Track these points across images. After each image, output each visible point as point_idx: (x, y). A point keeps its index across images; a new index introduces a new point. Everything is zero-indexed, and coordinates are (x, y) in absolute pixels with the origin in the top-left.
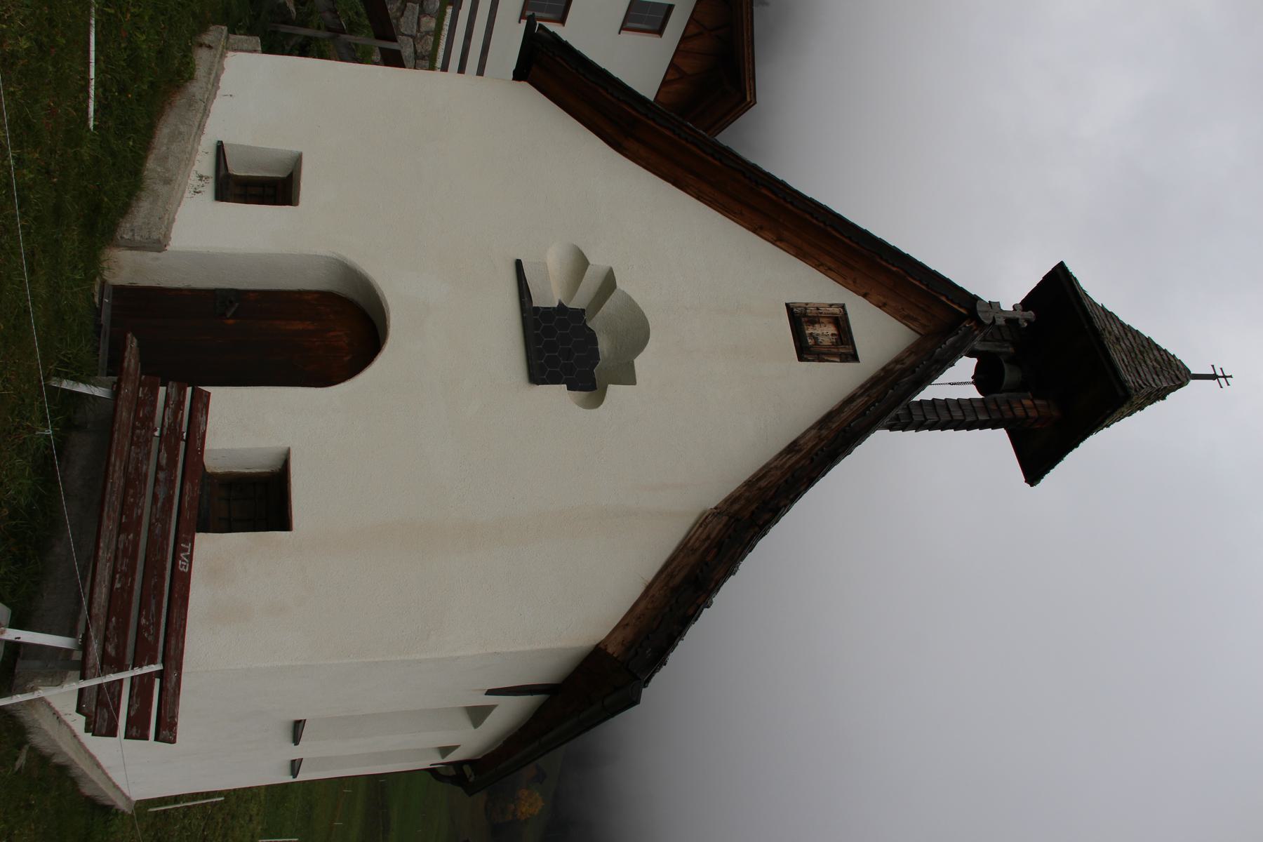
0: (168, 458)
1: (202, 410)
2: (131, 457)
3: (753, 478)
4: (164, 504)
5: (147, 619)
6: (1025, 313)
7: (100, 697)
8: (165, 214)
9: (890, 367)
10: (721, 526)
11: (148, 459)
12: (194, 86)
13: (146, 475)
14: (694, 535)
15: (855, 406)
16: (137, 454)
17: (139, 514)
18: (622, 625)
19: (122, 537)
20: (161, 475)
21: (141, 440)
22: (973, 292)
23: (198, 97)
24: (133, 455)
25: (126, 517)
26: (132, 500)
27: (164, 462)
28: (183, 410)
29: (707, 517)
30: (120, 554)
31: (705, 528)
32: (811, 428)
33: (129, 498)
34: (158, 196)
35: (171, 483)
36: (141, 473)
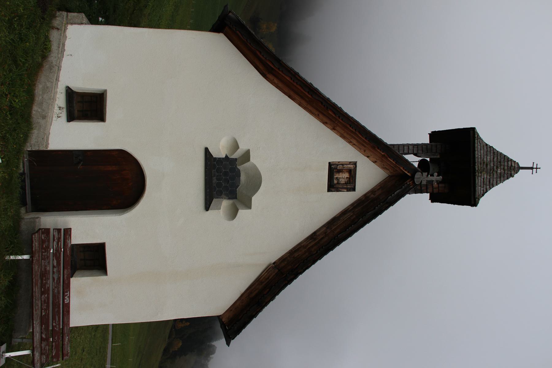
0: (57, 262)
1: (69, 238)
2: (43, 265)
3: (293, 250)
4: (57, 281)
5: (55, 323)
6: (438, 177)
7: (42, 352)
8: (44, 136)
9: (368, 195)
10: (274, 274)
11: (49, 264)
12: (52, 56)
13: (49, 271)
14: (264, 275)
15: (346, 217)
16: (45, 263)
17: (48, 286)
18: (229, 310)
19: (43, 296)
20: (55, 270)
21: (45, 257)
23: (54, 63)
24: (43, 264)
25: (43, 289)
26: (45, 282)
27: (55, 264)
28: (61, 241)
29: (270, 269)
30: (43, 303)
31: (268, 273)
33: (44, 281)
34: (41, 126)
35: (59, 272)
36: (47, 271)
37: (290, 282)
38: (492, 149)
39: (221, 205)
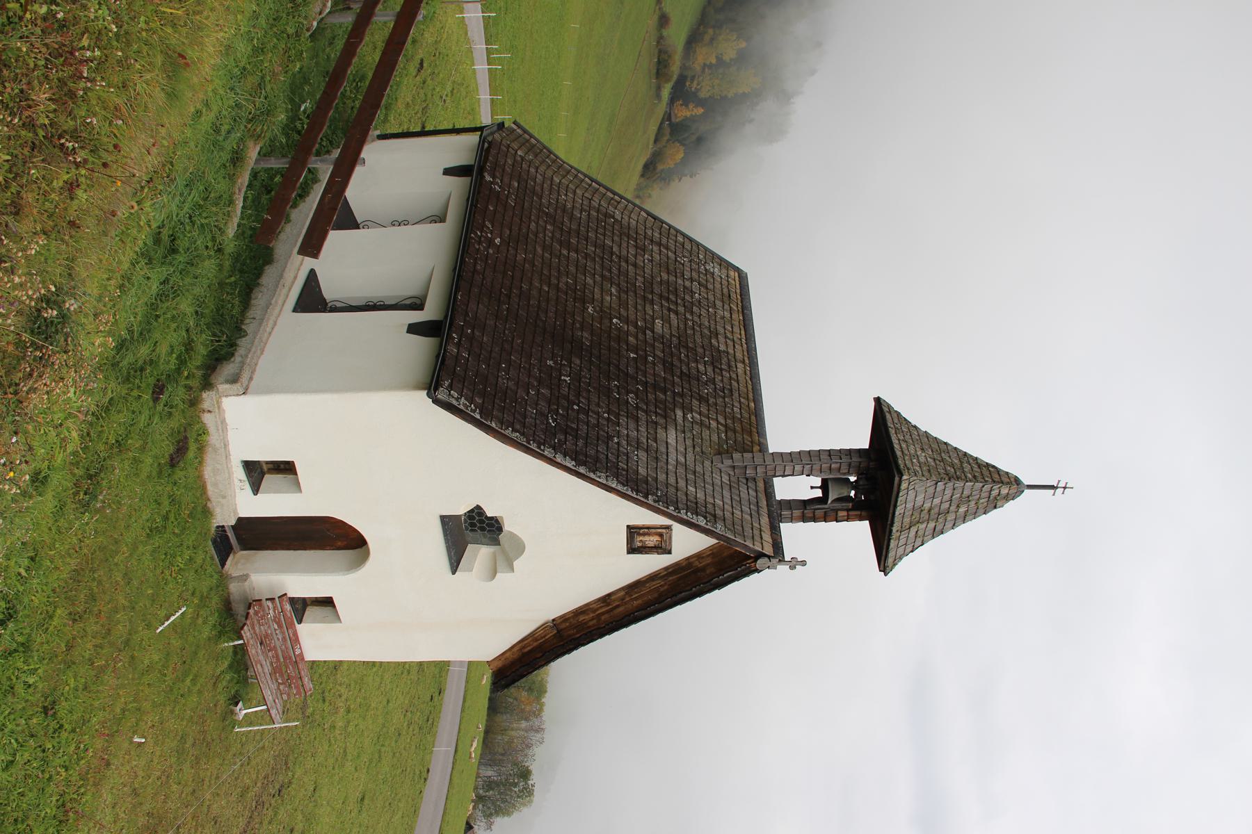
22: (873, 403)
32: (623, 589)
35: (283, 633)
37: (569, 651)
39: (476, 559)
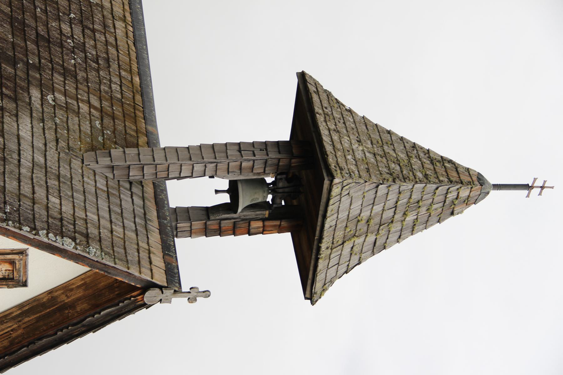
38: (308, 295)
